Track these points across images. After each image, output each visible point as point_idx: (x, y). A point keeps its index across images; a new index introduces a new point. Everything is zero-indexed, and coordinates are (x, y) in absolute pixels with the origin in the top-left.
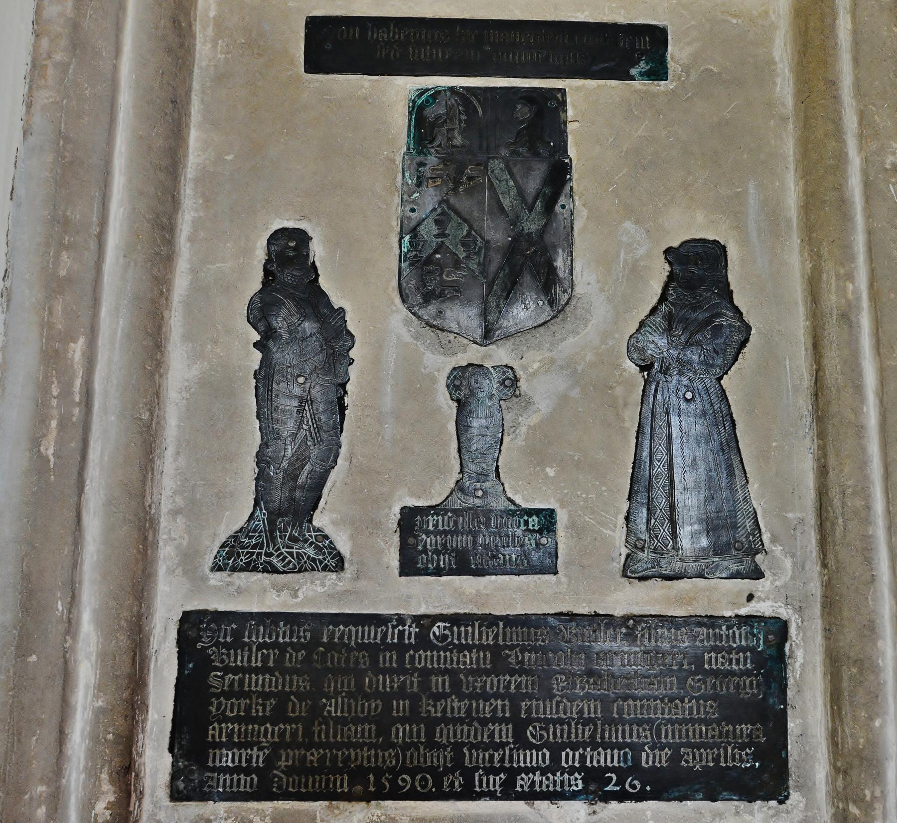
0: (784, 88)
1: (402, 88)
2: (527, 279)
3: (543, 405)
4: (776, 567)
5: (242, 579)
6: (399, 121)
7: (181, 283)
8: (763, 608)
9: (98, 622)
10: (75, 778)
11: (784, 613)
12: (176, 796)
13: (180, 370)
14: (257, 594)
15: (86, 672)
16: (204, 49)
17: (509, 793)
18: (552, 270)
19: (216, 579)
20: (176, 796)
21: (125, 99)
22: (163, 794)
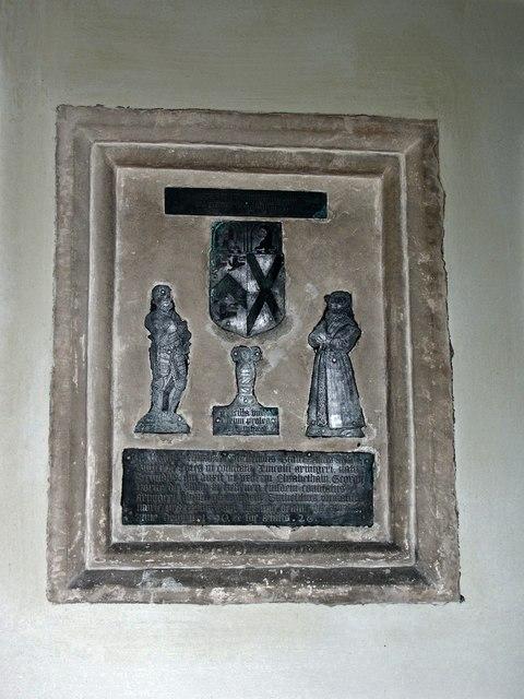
0: (378, 223)
1: (209, 221)
2: (265, 307)
3: (273, 364)
4: (370, 433)
5: (147, 436)
6: (208, 236)
7: (117, 309)
8: (364, 449)
9: (95, 450)
10: (89, 512)
11: (373, 451)
12: (124, 523)
13: (118, 348)
14: (156, 443)
15: (91, 471)
16: (120, 202)
17: (259, 522)
18: (276, 305)
19: (136, 436)
20: (124, 523)
21: (92, 229)
22: (119, 521)
